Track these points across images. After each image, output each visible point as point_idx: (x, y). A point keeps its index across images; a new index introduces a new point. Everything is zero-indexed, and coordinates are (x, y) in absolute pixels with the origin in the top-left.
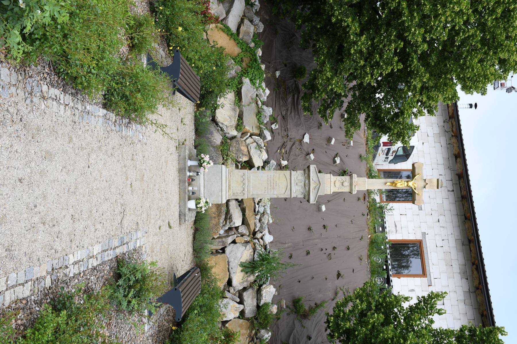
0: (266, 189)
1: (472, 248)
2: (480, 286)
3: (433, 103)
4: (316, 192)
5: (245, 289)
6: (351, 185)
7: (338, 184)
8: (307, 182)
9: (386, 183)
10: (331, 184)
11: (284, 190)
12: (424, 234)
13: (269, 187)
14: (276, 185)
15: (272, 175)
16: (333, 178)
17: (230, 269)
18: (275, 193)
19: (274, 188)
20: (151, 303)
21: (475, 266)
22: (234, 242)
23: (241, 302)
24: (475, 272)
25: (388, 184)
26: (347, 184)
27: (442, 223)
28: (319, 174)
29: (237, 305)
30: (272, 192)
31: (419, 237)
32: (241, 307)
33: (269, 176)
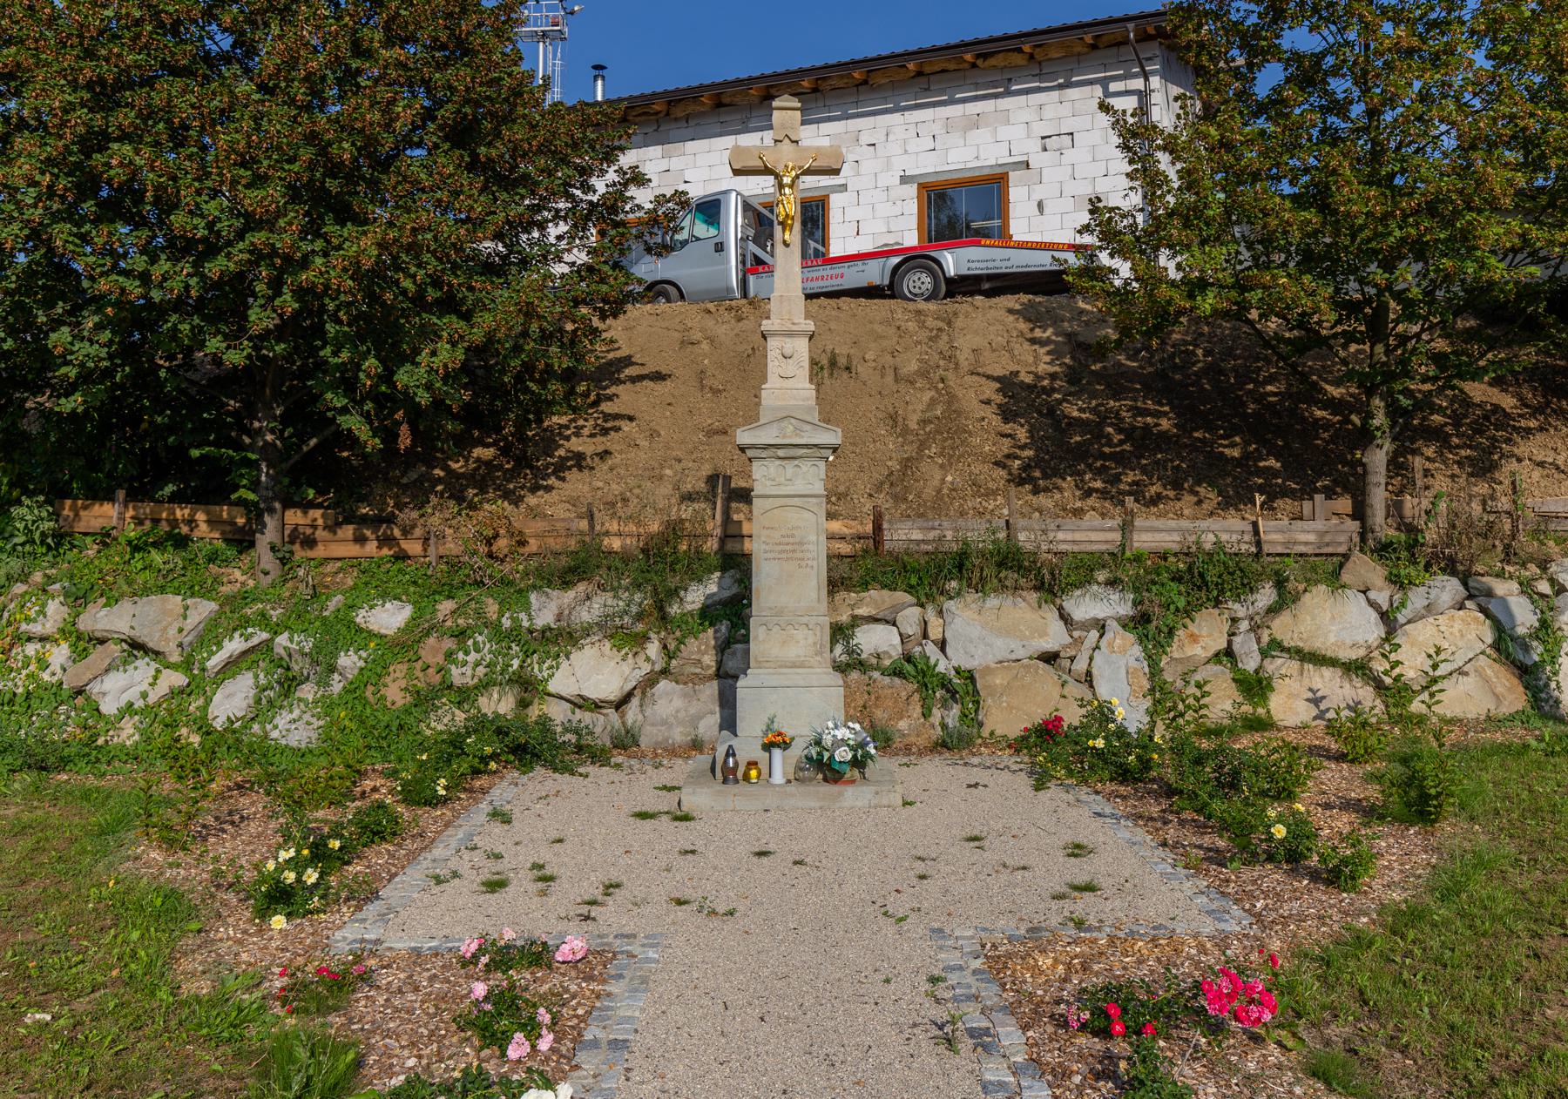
0: (803, 563)
1: (937, 68)
2: (1027, 48)
3: (814, 752)
4: (808, 427)
5: (1065, 618)
6: (791, 334)
7: (790, 368)
8: (781, 453)
9: (786, 244)
10: (788, 380)
11: (807, 515)
12: (905, 180)
13: (799, 555)
14: (793, 536)
15: (763, 547)
16: (773, 382)
17: (1014, 657)
18: (813, 538)
19: (801, 544)
20: (89, 54)
21: (979, 62)
22: (942, 645)
23: (1101, 626)
24: (992, 61)
25: (787, 236)
26: (790, 345)
27: (878, 137)
28: (762, 421)
29: (1109, 636)
30: (811, 547)
31: (912, 190)
32: (1113, 625)
33: (769, 555)
